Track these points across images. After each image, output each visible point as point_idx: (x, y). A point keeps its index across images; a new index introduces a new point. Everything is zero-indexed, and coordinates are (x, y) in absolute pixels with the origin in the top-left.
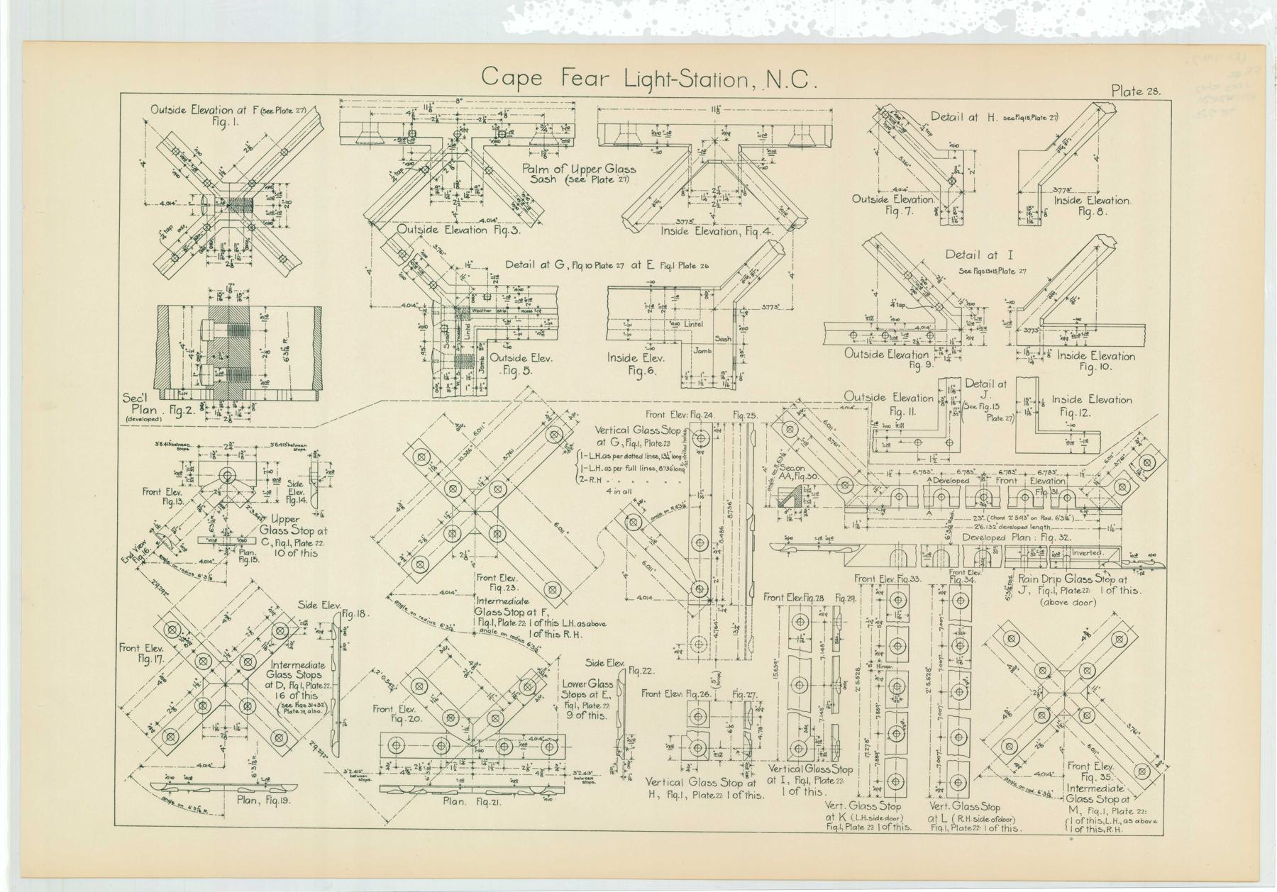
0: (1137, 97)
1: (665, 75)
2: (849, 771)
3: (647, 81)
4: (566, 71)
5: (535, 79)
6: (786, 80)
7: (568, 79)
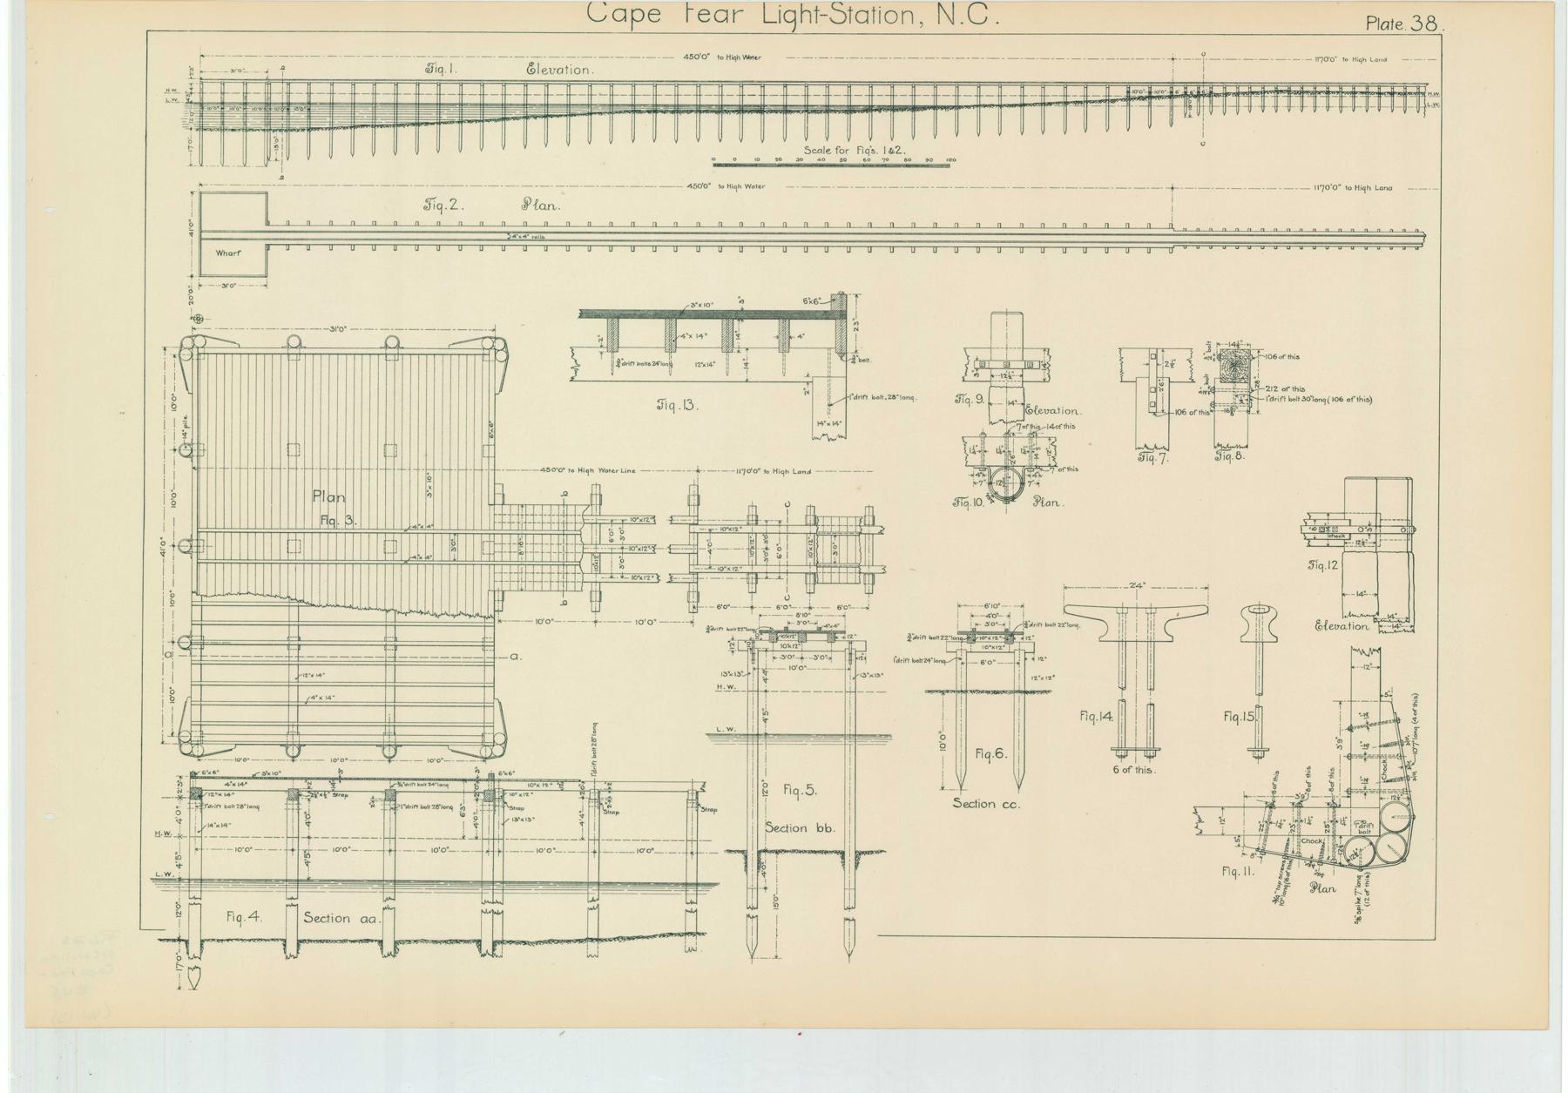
0: (1395, 31)
1: (812, 9)
2: (164, 880)
3: (790, 16)
5: (653, 14)
6: (961, 14)
7: (693, 15)
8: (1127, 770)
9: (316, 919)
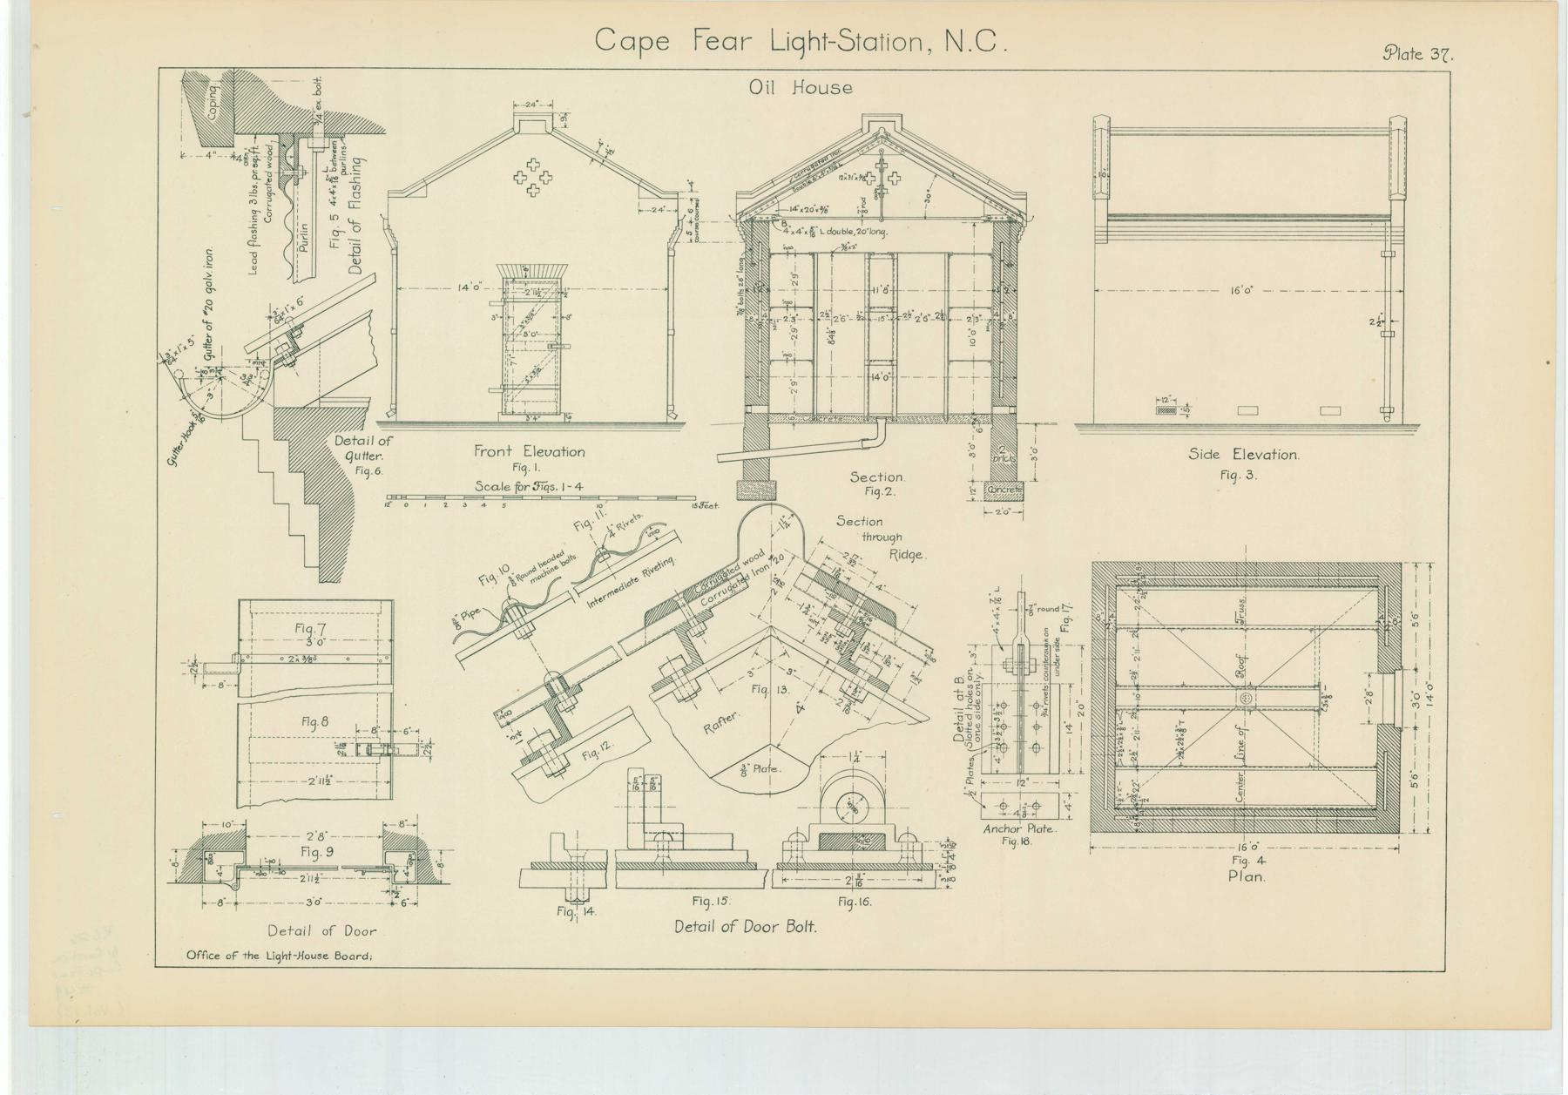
3: (798, 44)
4: (699, 32)
5: (661, 42)
6: (969, 42)
7: (702, 42)
8: (728, 928)
9: (849, 523)
